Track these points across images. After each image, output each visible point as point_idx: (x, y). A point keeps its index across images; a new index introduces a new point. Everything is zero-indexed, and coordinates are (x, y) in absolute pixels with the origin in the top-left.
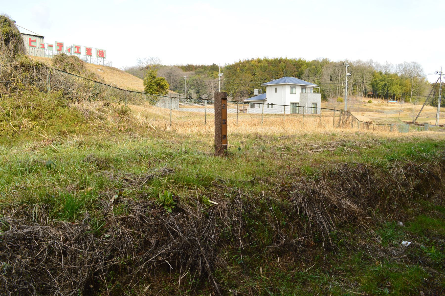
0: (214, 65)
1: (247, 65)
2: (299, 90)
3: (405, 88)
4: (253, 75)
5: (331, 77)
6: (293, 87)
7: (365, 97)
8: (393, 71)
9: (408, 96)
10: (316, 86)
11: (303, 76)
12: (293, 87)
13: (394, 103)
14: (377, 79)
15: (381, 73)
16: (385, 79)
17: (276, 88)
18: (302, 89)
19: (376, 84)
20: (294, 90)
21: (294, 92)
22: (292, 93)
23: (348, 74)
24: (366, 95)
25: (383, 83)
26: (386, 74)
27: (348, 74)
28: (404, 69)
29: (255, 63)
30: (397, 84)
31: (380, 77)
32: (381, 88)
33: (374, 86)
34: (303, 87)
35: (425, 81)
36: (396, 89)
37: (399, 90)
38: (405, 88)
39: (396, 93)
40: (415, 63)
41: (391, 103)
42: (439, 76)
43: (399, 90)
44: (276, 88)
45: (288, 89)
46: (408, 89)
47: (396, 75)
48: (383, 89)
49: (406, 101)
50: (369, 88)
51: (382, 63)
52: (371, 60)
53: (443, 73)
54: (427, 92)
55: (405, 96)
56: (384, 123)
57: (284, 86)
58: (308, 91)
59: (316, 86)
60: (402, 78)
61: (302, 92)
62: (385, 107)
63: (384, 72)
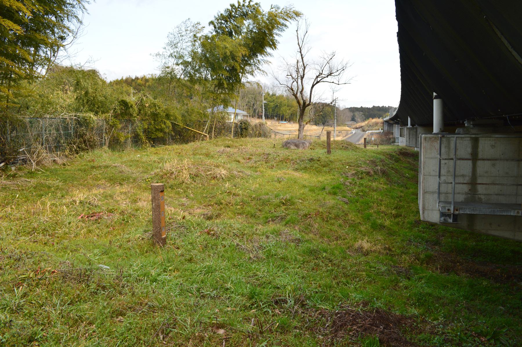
23: (264, 102)
26: (273, 95)
30: (285, 105)
41: (282, 123)
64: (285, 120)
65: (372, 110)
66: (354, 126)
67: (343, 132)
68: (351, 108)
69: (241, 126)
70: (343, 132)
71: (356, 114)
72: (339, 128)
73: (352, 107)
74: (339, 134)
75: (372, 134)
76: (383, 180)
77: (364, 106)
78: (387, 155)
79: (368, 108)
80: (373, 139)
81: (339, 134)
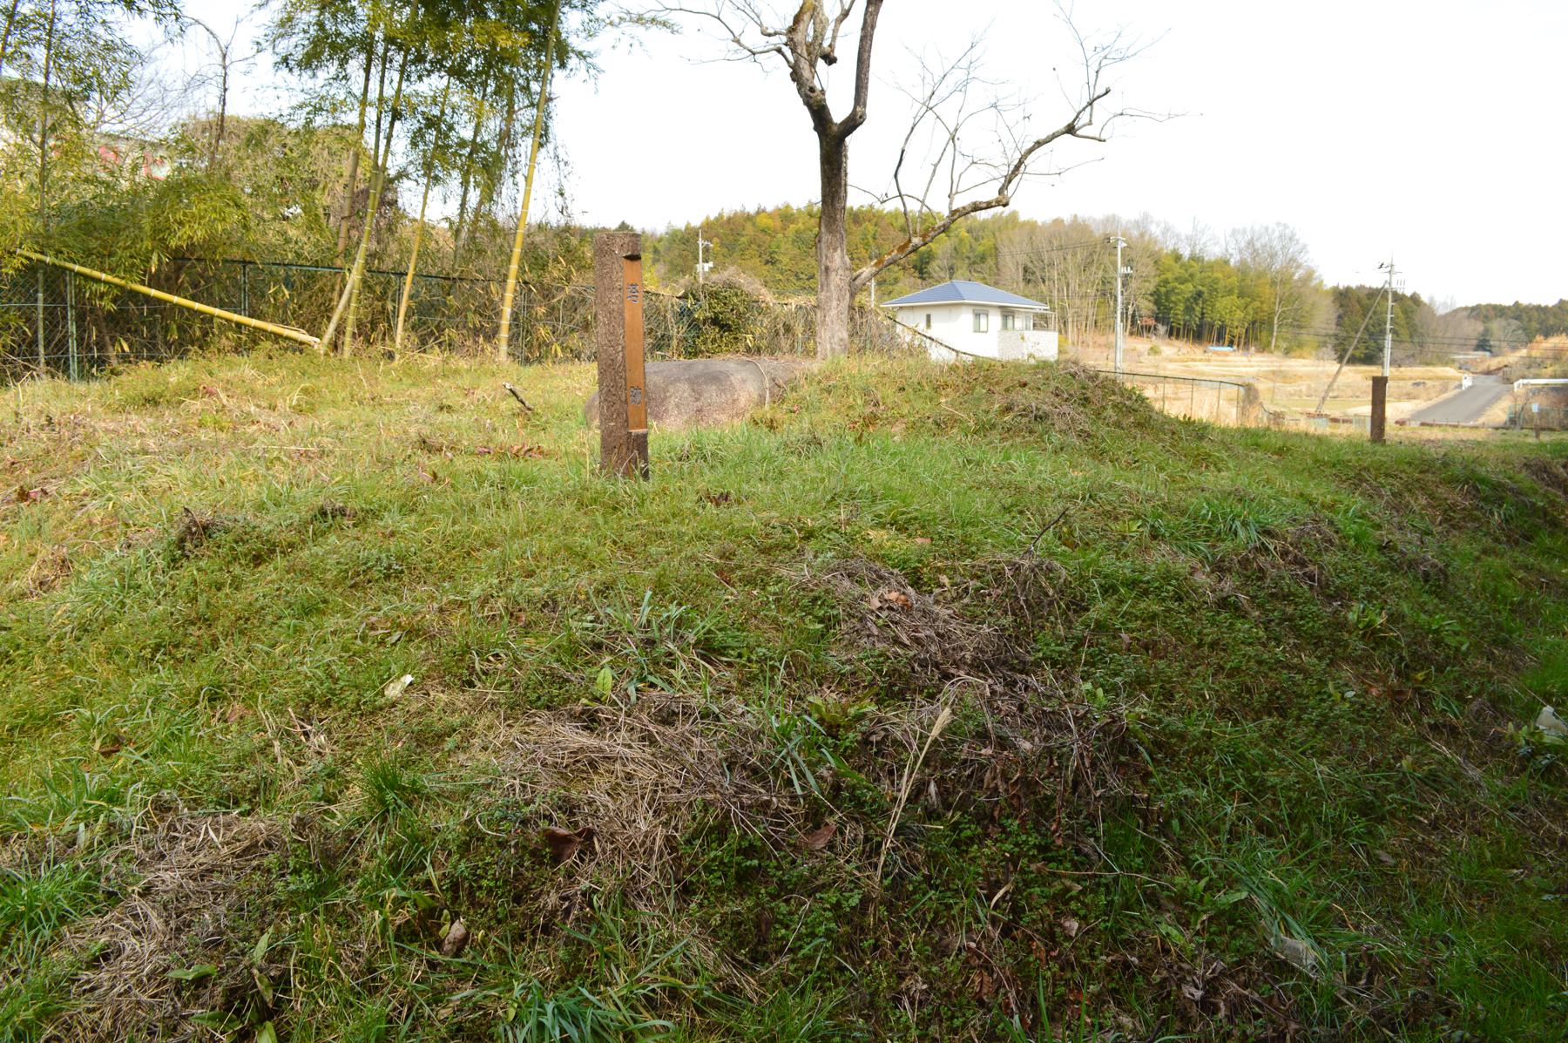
0: (623, 226)
1: (749, 230)
2: (995, 319)
3: (1257, 304)
4: (767, 262)
5: (1026, 270)
6: (980, 311)
7: (1131, 334)
8: (1213, 252)
9: (1264, 334)
10: (1040, 308)
11: (934, 266)
12: (980, 311)
13: (1226, 354)
14: (1169, 275)
15: (1178, 258)
16: (1191, 275)
17: (929, 317)
18: (1005, 317)
19: (1167, 293)
20: (983, 320)
21: (983, 328)
22: (977, 330)
23: (1123, 270)
24: (1137, 328)
25: (1188, 289)
26: (1193, 258)
27: (1123, 270)
28: (1251, 243)
29: (770, 222)
30: (1230, 292)
31: (1178, 271)
32: (1181, 307)
33: (1162, 301)
34: (1007, 313)
35: (1313, 283)
36: (1227, 309)
37: (1239, 314)
38: (1257, 304)
39: (1228, 322)
40: (1286, 226)
41: (1216, 353)
42: (1387, 277)
43: (1239, 314)
44: (929, 317)
45: (967, 317)
46: (1265, 307)
47: (1227, 262)
48: (1189, 310)
49: (1264, 348)
50: (1146, 306)
51: (1184, 228)
52: (1146, 216)
53: (1396, 269)
54: (1324, 317)
55: (1254, 335)
56: (1446, 407)
57: (954, 310)
58: (1019, 323)
59: (1040, 308)
60: (1243, 270)
61: (1005, 326)
62: (1200, 367)
63: (1186, 253)
64: (1231, 344)
65: (1555, 315)
66: (1483, 367)
67: (1429, 383)
68: (1478, 307)
69: (684, 313)
70: (1429, 383)
71: (1496, 325)
72: (1418, 371)
73: (1484, 303)
74: (1415, 391)
75: (1538, 391)
76: (526, 954)
77: (1524, 301)
78: (1452, 481)
79: (1538, 308)
80: (1535, 408)
81: (1415, 391)
